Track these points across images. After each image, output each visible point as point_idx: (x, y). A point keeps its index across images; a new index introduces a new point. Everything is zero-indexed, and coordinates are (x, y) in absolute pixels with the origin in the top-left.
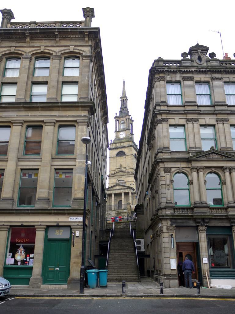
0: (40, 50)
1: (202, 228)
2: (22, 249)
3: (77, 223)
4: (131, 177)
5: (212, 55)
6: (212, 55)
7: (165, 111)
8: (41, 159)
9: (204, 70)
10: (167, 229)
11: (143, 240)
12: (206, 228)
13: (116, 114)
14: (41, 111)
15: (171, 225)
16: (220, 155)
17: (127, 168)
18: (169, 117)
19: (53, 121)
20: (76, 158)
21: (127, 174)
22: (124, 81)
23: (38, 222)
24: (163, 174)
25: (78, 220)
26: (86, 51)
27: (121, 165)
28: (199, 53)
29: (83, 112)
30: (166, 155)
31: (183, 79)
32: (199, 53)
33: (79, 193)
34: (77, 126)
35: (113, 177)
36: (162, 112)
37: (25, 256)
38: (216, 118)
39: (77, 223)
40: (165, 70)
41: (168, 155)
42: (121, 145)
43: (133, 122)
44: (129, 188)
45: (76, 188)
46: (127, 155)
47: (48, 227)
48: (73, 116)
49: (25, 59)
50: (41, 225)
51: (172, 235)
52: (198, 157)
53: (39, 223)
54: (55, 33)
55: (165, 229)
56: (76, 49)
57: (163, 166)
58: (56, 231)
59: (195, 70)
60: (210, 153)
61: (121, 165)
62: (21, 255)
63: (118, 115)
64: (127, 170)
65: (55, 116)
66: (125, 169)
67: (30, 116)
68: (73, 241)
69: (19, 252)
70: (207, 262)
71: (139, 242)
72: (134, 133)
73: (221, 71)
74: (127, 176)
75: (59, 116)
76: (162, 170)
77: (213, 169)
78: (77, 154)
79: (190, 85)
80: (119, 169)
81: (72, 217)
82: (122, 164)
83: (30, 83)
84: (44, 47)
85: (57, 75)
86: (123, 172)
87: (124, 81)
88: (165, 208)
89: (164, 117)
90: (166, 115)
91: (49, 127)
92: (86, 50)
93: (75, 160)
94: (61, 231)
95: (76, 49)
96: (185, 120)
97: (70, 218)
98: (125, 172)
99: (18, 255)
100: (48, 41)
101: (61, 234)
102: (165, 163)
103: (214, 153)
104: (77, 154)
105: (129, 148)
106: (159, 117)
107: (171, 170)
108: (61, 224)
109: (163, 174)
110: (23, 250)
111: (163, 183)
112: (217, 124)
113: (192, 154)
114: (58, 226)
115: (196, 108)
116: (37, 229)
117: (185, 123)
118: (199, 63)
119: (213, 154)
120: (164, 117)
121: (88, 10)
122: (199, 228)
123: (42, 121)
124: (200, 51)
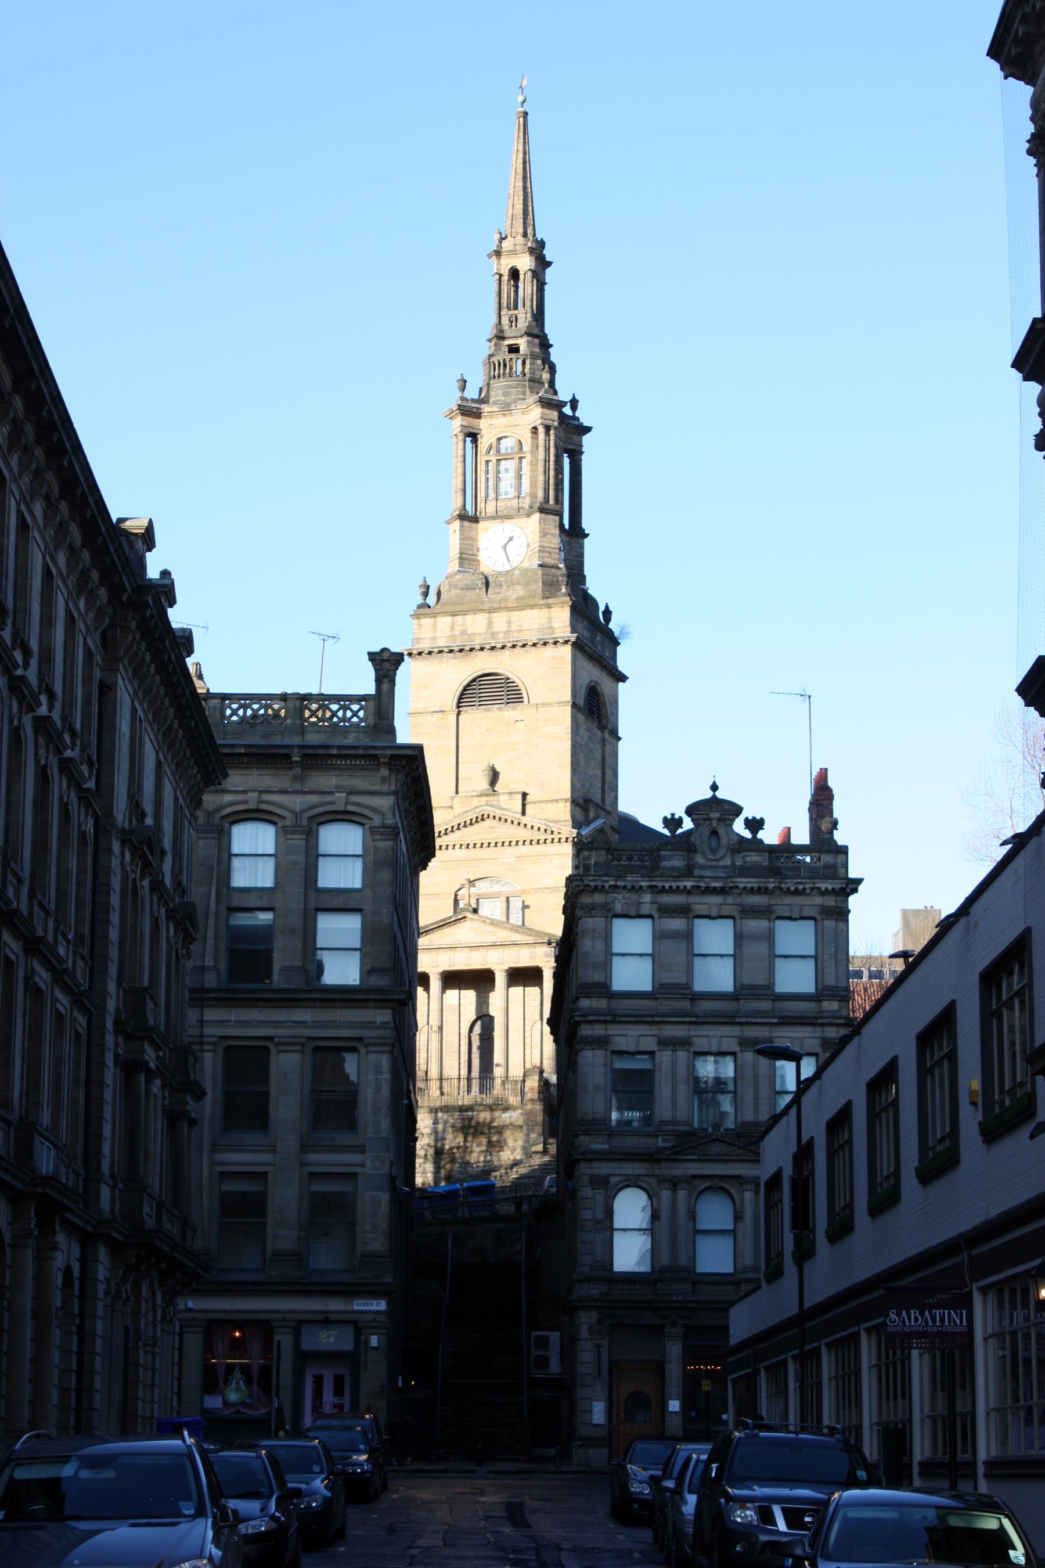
0: (245, 802)
1: (672, 1330)
2: (240, 1376)
3: (373, 1316)
5: (755, 825)
6: (755, 825)
7: (602, 1015)
8: (275, 1146)
9: (717, 884)
10: (590, 1330)
11: (558, 1334)
12: (683, 1330)
14: (265, 1007)
15: (600, 1321)
16: (734, 1145)
18: (613, 1030)
19: (299, 1040)
20: (364, 1146)
23: (277, 1312)
24: (588, 1192)
25: (374, 1308)
26: (384, 809)
28: (714, 823)
29: (378, 1012)
30: (599, 1143)
31: (659, 910)
32: (714, 823)
33: (147, 865)
34: (363, 1051)
36: (592, 1018)
37: (247, 1392)
38: (738, 1033)
39: (373, 1316)
40: (611, 886)
41: (603, 1143)
42: (490, 623)
43: (586, 439)
45: (367, 1228)
47: (300, 1322)
48: (353, 1025)
49: (204, 835)
50: (284, 1319)
51: (599, 1346)
52: (677, 1153)
53: (281, 1316)
54: (291, 758)
55: (584, 1333)
56: (353, 804)
57: (589, 1171)
58: (321, 1333)
59: (693, 887)
60: (711, 1141)
62: (238, 1390)
65: (303, 1024)
67: (236, 1022)
68: (363, 1357)
69: (231, 1383)
70: (677, 1409)
71: (544, 1343)
72: (586, 525)
73: (767, 888)
75: (315, 1025)
76: (585, 1180)
77: (715, 1181)
78: (367, 1136)
79: (676, 931)
81: (359, 1302)
83: (223, 909)
84: (257, 794)
85: (302, 890)
88: (588, 1280)
89: (598, 1030)
90: (603, 1026)
91: (289, 1056)
92: (382, 806)
93: (361, 1149)
94: (331, 1332)
95: (353, 804)
96: (654, 1040)
97: (355, 1302)
99: (231, 1390)
100: (268, 772)
101: (331, 1340)
102: (595, 1164)
103: (720, 1141)
104: (367, 1136)
106: (586, 1031)
107: (608, 1182)
108: (333, 1317)
109: (588, 1192)
110: (242, 1379)
111: (586, 1215)
112: (742, 1051)
113: (663, 1141)
114: (326, 1321)
115: (685, 1005)
116: (276, 1330)
117: (655, 1048)
118: (712, 857)
119: (717, 1142)
120: (598, 1030)
121: (386, 655)
122: (666, 1330)
123: (271, 1038)
124: (717, 815)
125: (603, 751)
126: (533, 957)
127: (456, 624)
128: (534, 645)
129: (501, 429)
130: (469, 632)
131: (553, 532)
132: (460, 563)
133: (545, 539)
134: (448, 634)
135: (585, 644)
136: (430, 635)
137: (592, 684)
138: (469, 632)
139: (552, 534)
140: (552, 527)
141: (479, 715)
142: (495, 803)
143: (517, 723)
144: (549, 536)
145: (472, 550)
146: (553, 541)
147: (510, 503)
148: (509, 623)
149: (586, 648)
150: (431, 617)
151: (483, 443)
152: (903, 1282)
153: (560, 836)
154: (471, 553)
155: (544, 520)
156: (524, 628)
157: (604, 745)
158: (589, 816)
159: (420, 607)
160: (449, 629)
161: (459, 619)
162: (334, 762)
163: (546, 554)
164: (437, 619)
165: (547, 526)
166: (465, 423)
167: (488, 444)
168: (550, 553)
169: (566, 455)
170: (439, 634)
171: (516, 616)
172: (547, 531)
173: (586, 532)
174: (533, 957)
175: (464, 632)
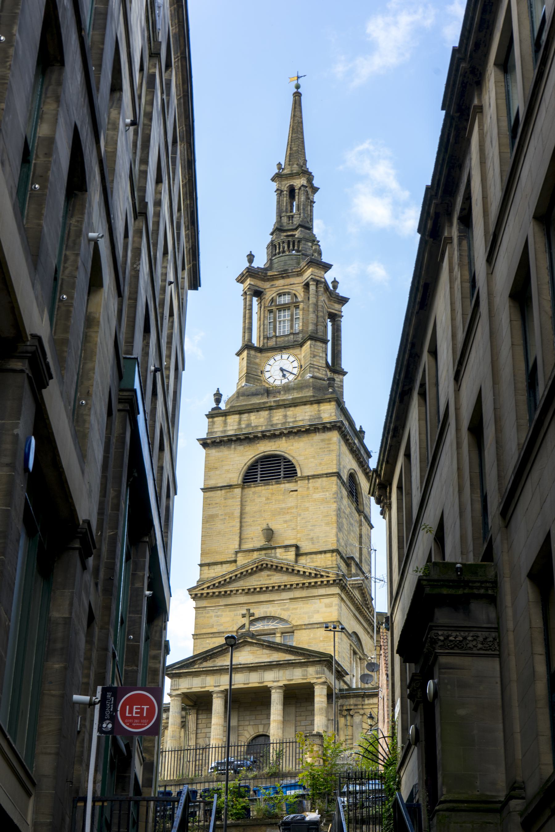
4: (327, 601)
13: (251, 258)
17: (306, 547)
21: (295, 580)
22: (297, 95)
27: (269, 533)
35: (222, 601)
44: (313, 663)
46: (308, 478)
61: (269, 533)
63: (260, 262)
64: (303, 560)
66: (291, 555)
72: (345, 365)
74: (304, 593)
80: (256, 555)
82: (273, 526)
86: (278, 569)
87: (297, 95)
98: (292, 572)
105: (317, 437)
125: (361, 530)
126: (305, 676)
127: (242, 419)
128: (298, 87)
129: (280, 288)
130: (253, 425)
131: (321, 355)
132: (246, 380)
133: (314, 359)
134: (236, 427)
135: (348, 432)
136: (221, 429)
137: (352, 471)
138: (253, 425)
139: (320, 357)
140: (320, 351)
141: (260, 488)
142: (273, 555)
143: (292, 493)
144: (318, 358)
145: (257, 372)
146: (321, 361)
147: (286, 339)
148: (285, 416)
149: (348, 437)
150: (222, 416)
151: (267, 298)
152: (83, 593)
153: (328, 579)
154: (255, 374)
155: (314, 345)
156: (297, 419)
157: (361, 525)
158: (351, 571)
159: (213, 409)
160: (236, 424)
161: (245, 416)
162: (351, 788)
163: (316, 370)
164: (228, 417)
165: (316, 350)
166: (252, 283)
167: (270, 298)
168: (319, 369)
169: (329, 320)
170: (229, 428)
171: (290, 412)
172: (315, 353)
173: (345, 370)
174: (305, 676)
175: (248, 425)
